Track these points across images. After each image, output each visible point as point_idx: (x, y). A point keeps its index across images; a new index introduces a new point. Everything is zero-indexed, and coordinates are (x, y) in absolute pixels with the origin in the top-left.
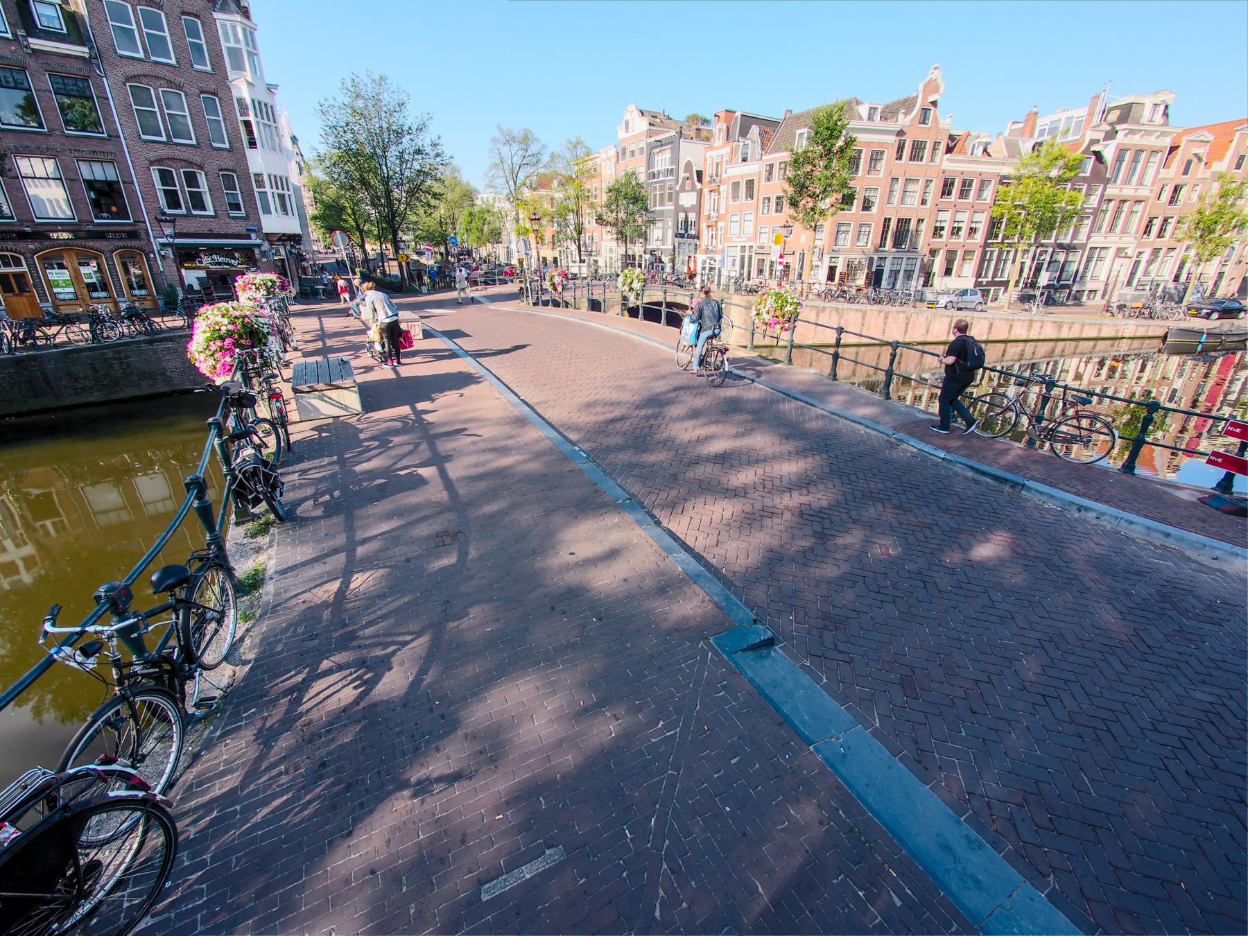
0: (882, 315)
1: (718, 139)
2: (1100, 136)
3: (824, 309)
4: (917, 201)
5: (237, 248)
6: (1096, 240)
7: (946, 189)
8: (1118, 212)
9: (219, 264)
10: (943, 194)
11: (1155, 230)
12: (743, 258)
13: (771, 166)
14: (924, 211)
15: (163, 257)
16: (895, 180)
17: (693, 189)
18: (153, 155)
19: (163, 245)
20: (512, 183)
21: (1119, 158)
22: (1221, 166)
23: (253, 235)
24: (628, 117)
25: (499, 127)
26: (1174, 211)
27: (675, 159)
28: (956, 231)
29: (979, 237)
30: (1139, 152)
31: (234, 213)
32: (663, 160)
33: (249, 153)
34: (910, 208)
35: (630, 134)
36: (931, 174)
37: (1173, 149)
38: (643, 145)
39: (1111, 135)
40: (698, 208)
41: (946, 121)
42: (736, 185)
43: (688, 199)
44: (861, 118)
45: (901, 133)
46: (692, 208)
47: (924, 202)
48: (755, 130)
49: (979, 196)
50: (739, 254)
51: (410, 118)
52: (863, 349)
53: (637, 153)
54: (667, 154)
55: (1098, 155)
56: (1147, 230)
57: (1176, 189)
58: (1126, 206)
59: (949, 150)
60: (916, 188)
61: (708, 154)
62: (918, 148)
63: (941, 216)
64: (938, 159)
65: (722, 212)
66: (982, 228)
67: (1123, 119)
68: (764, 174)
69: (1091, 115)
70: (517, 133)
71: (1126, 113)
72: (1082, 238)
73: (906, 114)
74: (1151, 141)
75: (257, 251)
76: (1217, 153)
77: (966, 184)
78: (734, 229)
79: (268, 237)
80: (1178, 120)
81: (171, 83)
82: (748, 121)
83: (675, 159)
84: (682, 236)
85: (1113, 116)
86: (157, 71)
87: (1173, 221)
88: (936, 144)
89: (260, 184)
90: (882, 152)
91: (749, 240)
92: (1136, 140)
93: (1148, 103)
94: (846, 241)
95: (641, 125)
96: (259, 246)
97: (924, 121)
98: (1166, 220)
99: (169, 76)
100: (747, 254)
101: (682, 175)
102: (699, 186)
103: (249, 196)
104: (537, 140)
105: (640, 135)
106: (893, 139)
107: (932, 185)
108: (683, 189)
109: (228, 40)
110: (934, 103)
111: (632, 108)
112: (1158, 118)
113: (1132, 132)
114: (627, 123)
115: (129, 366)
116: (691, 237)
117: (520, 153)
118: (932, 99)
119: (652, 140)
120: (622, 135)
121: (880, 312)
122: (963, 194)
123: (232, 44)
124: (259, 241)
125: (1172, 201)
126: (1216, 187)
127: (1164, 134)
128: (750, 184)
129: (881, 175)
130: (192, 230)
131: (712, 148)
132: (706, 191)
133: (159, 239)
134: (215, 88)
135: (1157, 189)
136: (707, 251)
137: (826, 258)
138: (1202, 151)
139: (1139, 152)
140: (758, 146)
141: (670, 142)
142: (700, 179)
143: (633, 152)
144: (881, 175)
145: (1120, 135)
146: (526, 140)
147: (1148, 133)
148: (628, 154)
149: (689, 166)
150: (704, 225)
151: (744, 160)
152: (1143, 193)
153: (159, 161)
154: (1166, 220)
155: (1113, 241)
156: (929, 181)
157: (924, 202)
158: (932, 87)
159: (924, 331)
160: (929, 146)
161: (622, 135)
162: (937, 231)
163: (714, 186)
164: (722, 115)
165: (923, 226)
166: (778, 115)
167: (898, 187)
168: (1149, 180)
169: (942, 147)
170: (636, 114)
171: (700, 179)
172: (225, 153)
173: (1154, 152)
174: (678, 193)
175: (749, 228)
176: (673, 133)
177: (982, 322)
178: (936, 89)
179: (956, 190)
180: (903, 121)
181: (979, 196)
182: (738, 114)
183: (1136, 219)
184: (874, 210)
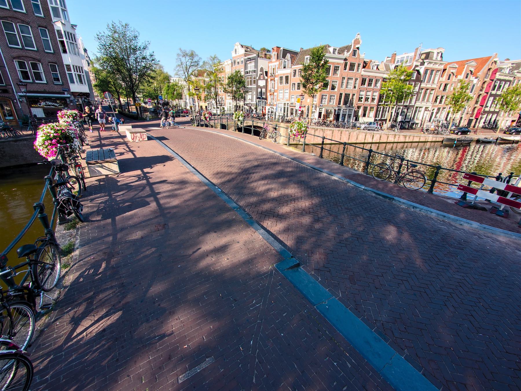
0: (340, 132)
1: (274, 59)
2: (419, 64)
3: (317, 129)
4: (352, 87)
5: (58, 98)
6: (418, 104)
7: (363, 82)
8: (431, 74)
9: (50, 105)
10: (362, 84)
11: (438, 100)
12: (285, 108)
13: (295, 71)
15: (21, 102)
16: (344, 78)
17: (264, 79)
18: (15, 55)
20: (186, 73)
21: (426, 73)
24: (236, 47)
25: (180, 49)
26: (445, 94)
27: (256, 66)
28: (367, 99)
29: (376, 102)
31: (56, 83)
32: (251, 66)
33: (63, 55)
35: (237, 55)
36: (357, 76)
37: (444, 70)
39: (422, 64)
40: (266, 87)
41: (363, 55)
42: (281, 78)
43: (262, 83)
44: (330, 53)
45: (345, 60)
46: (264, 87)
47: (355, 87)
48: (288, 56)
49: (375, 85)
50: (283, 106)
51: (140, 43)
53: (240, 63)
54: (253, 64)
55: (418, 71)
56: (436, 101)
57: (446, 85)
58: (428, 91)
60: (352, 82)
61: (270, 65)
62: (352, 66)
63: (362, 93)
64: (360, 70)
65: (276, 88)
66: (377, 98)
68: (292, 74)
69: (415, 56)
70: (188, 52)
71: (428, 55)
73: (348, 52)
74: (437, 67)
75: (68, 100)
76: (459, 73)
77: (371, 81)
78: (281, 96)
79: (73, 94)
80: (446, 60)
81: (23, 22)
82: (285, 52)
83: (256, 66)
84: (259, 98)
85: (423, 57)
86: (16, 15)
87: (445, 97)
89: (69, 69)
90: (339, 67)
91: (287, 100)
92: (431, 66)
94: (325, 102)
95: (242, 51)
96: (69, 98)
97: (354, 55)
98: (442, 97)
100: (286, 106)
101: (259, 73)
102: (266, 78)
103: (63, 75)
104: (197, 55)
105: (241, 55)
106: (342, 62)
107: (358, 81)
108: (259, 79)
110: (358, 48)
111: (238, 44)
112: (439, 58)
113: (430, 63)
114: (236, 50)
115: (4, 152)
116: (263, 98)
117: (190, 61)
118: (357, 46)
119: (246, 58)
120: (234, 55)
121: (339, 131)
122: (370, 84)
123: (54, 5)
124: (69, 96)
127: (441, 64)
128: (287, 77)
130: (35, 90)
131: (271, 62)
132: (269, 80)
133: (19, 94)
134: (46, 25)
135: (439, 85)
137: (318, 109)
138: (454, 71)
139: (432, 71)
140: (290, 62)
141: (254, 59)
142: (267, 75)
143: (238, 63)
145: (426, 64)
146: (192, 55)
147: (436, 63)
148: (236, 63)
150: (268, 94)
151: (285, 67)
152: (434, 86)
154: (442, 97)
155: (424, 105)
156: (356, 79)
157: (355, 87)
158: (357, 42)
161: (234, 55)
162: (360, 99)
163: (272, 78)
164: (275, 49)
165: (355, 97)
166: (298, 50)
167: (345, 81)
168: (438, 80)
169: (361, 66)
170: (240, 46)
171: (267, 75)
172: (51, 55)
174: (257, 80)
175: (287, 96)
178: (359, 43)
180: (346, 55)
181: (375, 85)
182: (282, 49)
183: (432, 96)
184: (336, 90)
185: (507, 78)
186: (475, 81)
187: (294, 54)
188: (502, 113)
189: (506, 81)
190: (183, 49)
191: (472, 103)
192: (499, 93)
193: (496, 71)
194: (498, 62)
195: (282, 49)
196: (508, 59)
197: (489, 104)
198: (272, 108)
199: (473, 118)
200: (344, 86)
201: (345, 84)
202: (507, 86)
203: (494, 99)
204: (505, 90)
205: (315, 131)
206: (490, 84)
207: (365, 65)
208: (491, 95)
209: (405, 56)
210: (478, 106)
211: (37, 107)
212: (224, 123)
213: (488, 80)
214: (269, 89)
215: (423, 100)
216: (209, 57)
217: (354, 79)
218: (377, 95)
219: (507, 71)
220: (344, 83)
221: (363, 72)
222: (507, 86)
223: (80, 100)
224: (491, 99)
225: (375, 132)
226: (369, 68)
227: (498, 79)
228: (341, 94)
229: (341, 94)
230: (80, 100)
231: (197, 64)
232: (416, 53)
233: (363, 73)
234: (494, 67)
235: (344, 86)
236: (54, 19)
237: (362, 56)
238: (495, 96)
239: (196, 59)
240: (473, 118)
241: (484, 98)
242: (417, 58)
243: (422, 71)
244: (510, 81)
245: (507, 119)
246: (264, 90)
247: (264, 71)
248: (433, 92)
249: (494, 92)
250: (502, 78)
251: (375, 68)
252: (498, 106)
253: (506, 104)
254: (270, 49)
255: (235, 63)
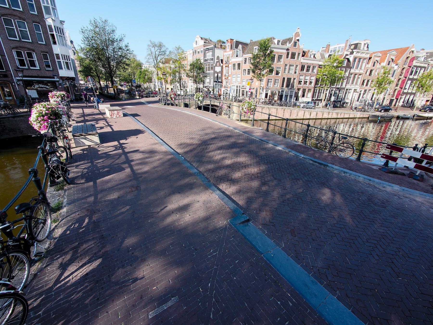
0: (283, 110)
1: (228, 49)
2: (349, 53)
3: (264, 107)
5: (49, 82)
6: (348, 87)
7: (302, 68)
8: (359, 61)
11: (365, 84)
12: (237, 90)
13: (246, 59)
14: (295, 76)
15: (18, 85)
16: (286, 65)
17: (220, 65)
18: (13, 45)
19: (18, 80)
20: (155, 61)
22: (384, 64)
23: (55, 77)
24: (197, 39)
25: (150, 41)
26: (371, 78)
27: (213, 55)
28: (305, 83)
29: (313, 85)
30: (360, 59)
32: (209, 55)
34: (291, 74)
35: (198, 45)
36: (298, 63)
38: (202, 49)
39: (352, 53)
41: (302, 46)
42: (234, 65)
43: (218, 69)
44: (275, 44)
45: (288, 49)
46: (219, 72)
47: (295, 73)
48: (240, 46)
52: (277, 121)
53: (200, 52)
56: (363, 84)
58: (357, 76)
59: (303, 56)
61: (225, 54)
63: (301, 77)
64: (300, 58)
65: (230, 74)
66: (314, 82)
67: (355, 48)
68: (244, 62)
69: (346, 46)
70: (157, 43)
71: (356, 46)
72: (344, 86)
73: (289, 43)
74: (364, 55)
75: (57, 83)
76: (382, 60)
77: (309, 67)
78: (234, 79)
79: (62, 78)
80: (371, 50)
81: (20, 18)
82: (238, 43)
83: (213, 55)
84: (216, 82)
85: (353, 47)
86: (15, 13)
87: (370, 81)
88: (299, 54)
89: (58, 58)
90: (282, 56)
91: (239, 84)
92: (359, 55)
93: (363, 43)
94: (271, 85)
95: (202, 43)
96: (58, 81)
97: (295, 45)
98: (368, 81)
99: (20, 15)
100: (238, 88)
101: (216, 61)
102: (222, 65)
103: (53, 61)
104: (164, 46)
106: (285, 51)
108: (216, 66)
109: (44, 3)
110: (298, 40)
111: (198, 36)
113: (358, 52)
114: (196, 42)
115: (5, 126)
116: (219, 82)
118: (297, 39)
119: (205, 48)
120: (195, 45)
121: (282, 109)
122: (308, 70)
123: (46, 5)
124: (58, 79)
125: (370, 74)
126: (382, 71)
127: (367, 53)
128: (239, 65)
129: (282, 63)
130: (30, 75)
132: (224, 66)
133: (17, 78)
135: (365, 71)
136: (225, 87)
137: (265, 90)
138: (378, 59)
139: (360, 59)
140: (241, 52)
141: (211, 49)
142: (222, 63)
143: (199, 52)
144: (282, 63)
145: (355, 53)
147: (363, 53)
148: (197, 52)
149: (218, 57)
150: (224, 78)
151: (237, 56)
152: (361, 72)
153: (16, 48)
154: (368, 81)
155: (353, 87)
156: (297, 66)
157: (295, 73)
158: (297, 34)
159: (296, 115)
160: (297, 54)
161: (195, 45)
163: (227, 65)
164: (229, 40)
165: (295, 81)
166: (248, 42)
167: (287, 67)
168: (365, 67)
169: (301, 55)
170: (200, 39)
171: (222, 63)
173: (365, 59)
174: (214, 67)
175: (239, 79)
176: (212, 46)
177: (314, 112)
178: (299, 36)
179: (305, 69)
180: (288, 45)
182: (235, 40)
183: (359, 80)
184: (280, 75)
185: (422, 65)
186: (396, 67)
187: (245, 45)
188: (418, 94)
189: (421, 67)
190: (152, 41)
191: (393, 85)
192: (415, 77)
193: (413, 59)
194: (415, 52)
195: (235, 40)
196: (423, 49)
197: (407, 87)
198: (226, 90)
199: (394, 98)
200: (287, 72)
201: (287, 70)
202: (422, 71)
203: (412, 82)
204: (420, 75)
205: (262, 109)
206: (408, 69)
207: (304, 54)
208: (409, 79)
209: (338, 46)
210: (398, 88)
211: (32, 89)
212: (186, 103)
213: (406, 66)
214: (224, 74)
215: (352, 83)
216: (174, 47)
217: (295, 66)
218: (314, 79)
219: (422, 59)
220: (285, 68)
221: (302, 60)
222: (422, 71)
223: (68, 84)
224: (409, 82)
225: (312, 110)
226: (307, 56)
227: (415, 66)
228: (284, 79)
229: (284, 79)
230: (68, 84)
231: (164, 52)
232: (346, 44)
233: (302, 61)
234: (412, 56)
235: (287, 72)
236: (46, 16)
237: (301, 47)
238: (412, 80)
239: (163, 49)
240: (394, 98)
241: (403, 82)
242: (347, 48)
243: (351, 59)
244: (425, 68)
245: (422, 99)
246: (220, 75)
247: (220, 59)
248: (360, 76)
249: (411, 77)
250: (418, 65)
251: (312, 56)
252: (415, 88)
253: (422, 86)
254: (225, 41)
255: (196, 52)
